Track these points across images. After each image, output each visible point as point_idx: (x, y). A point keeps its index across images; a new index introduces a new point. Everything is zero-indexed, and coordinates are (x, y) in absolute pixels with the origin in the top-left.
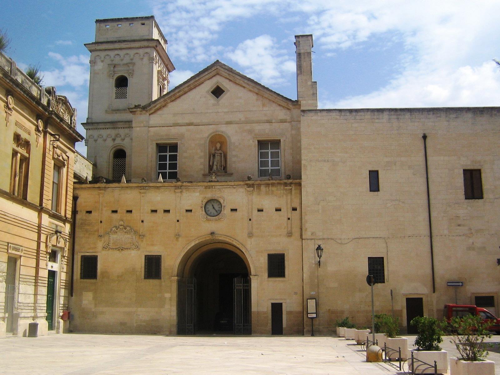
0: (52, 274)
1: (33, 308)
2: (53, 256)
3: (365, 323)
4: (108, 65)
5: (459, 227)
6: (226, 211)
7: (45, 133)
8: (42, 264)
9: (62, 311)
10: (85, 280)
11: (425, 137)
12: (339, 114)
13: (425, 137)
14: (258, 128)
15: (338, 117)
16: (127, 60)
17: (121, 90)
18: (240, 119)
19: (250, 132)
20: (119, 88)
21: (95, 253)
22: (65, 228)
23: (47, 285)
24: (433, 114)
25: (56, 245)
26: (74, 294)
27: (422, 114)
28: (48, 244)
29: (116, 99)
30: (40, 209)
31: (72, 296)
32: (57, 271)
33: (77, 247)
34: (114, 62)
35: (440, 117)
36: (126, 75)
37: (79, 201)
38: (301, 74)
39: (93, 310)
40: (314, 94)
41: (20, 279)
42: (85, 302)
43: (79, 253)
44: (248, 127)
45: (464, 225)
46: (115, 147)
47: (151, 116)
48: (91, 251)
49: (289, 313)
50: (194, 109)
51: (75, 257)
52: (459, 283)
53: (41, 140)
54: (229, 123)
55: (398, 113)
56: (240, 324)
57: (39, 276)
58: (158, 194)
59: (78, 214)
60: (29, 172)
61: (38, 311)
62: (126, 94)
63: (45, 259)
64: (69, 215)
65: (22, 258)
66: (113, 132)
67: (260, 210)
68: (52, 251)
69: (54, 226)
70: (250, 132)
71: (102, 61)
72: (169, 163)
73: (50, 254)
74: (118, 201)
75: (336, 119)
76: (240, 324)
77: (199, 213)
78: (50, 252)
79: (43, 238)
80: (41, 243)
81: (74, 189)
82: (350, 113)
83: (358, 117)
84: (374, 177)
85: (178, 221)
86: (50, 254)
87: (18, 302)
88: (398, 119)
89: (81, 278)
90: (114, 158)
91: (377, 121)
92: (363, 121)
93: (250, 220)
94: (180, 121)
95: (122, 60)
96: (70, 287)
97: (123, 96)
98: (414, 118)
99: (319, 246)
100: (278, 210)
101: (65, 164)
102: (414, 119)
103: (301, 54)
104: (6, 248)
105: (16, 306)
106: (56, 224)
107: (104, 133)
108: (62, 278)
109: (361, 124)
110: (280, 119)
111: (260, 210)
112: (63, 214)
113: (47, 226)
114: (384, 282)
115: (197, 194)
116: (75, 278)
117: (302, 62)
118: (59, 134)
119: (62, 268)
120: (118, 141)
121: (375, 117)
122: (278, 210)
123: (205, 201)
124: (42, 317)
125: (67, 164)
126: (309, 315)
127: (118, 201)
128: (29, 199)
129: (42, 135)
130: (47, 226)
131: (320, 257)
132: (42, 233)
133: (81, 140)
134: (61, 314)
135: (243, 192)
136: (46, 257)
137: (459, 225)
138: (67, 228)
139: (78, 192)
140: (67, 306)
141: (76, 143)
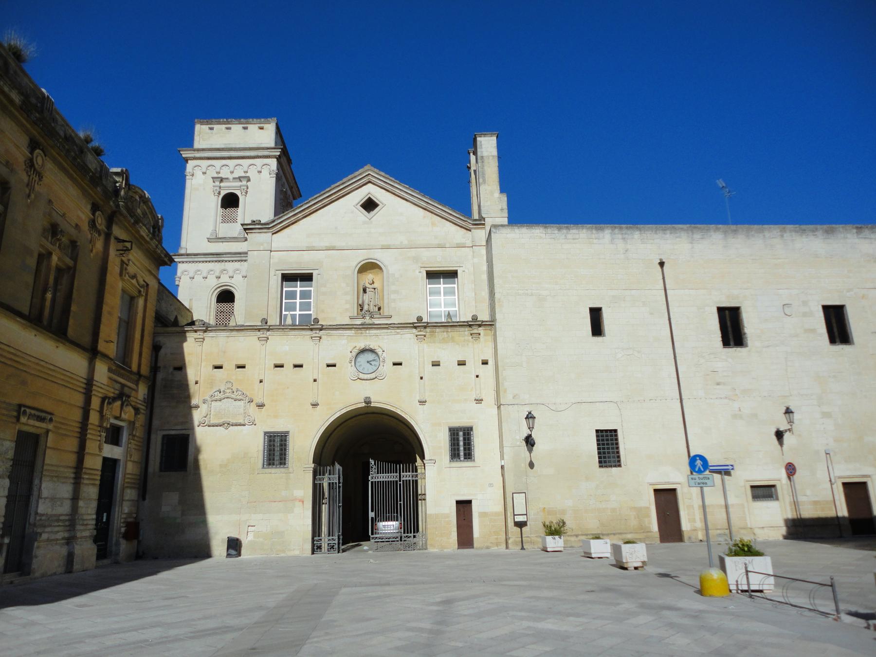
0: (110, 465)
1: (67, 523)
2: (114, 436)
3: (598, 528)
4: (213, 178)
5: (718, 387)
6: (387, 368)
7: (108, 236)
8: (91, 446)
9: (124, 525)
10: (166, 473)
11: (662, 264)
12: (544, 232)
13: (662, 264)
14: (426, 254)
15: (544, 236)
16: (239, 173)
17: (225, 306)
18: (402, 242)
19: (416, 259)
20: (227, 210)
21: (184, 431)
22: (137, 391)
23: (98, 482)
24: (671, 233)
25: (118, 415)
26: (147, 497)
27: (656, 233)
28: (104, 414)
29: (222, 224)
30: (93, 352)
31: (144, 499)
32: (119, 460)
33: (156, 423)
34: (220, 175)
35: (680, 237)
36: (238, 193)
37: (162, 352)
38: (485, 183)
39: (178, 521)
40: (503, 209)
41: (515, 517)
42: (165, 509)
43: (159, 432)
44: (413, 252)
45: (724, 384)
46: (219, 287)
47: (274, 235)
48: (179, 427)
49: (483, 515)
50: (336, 228)
51: (153, 437)
52: (727, 466)
53: (99, 245)
54: (388, 247)
55: (624, 232)
56: (409, 535)
57: (84, 467)
58: (285, 341)
59: (160, 371)
60: (74, 291)
61: (78, 527)
62: (229, 321)
63: (99, 438)
64: (145, 370)
65: (50, 434)
66: (217, 267)
67: (436, 364)
68: (110, 426)
69: (118, 386)
70: (416, 259)
71: (204, 173)
72: (300, 302)
73: (107, 430)
74: (225, 352)
75: (541, 238)
76: (409, 535)
77: (347, 369)
78: (108, 426)
79: (95, 403)
80: (92, 412)
81: (155, 334)
82: (558, 231)
83: (569, 236)
84: (596, 314)
85: (315, 381)
86: (107, 430)
87: (36, 513)
88: (625, 239)
89: (161, 470)
90: (217, 302)
91: (595, 241)
92: (577, 240)
93: (421, 378)
94: (317, 243)
95: (232, 172)
96: (143, 485)
97: (228, 310)
98: (645, 238)
99: (530, 413)
100: (462, 363)
101: (142, 293)
102: (645, 240)
103: (484, 158)
104: (15, 414)
105: (32, 520)
106: (120, 383)
107: (204, 267)
108: (128, 470)
109: (574, 245)
110: (457, 243)
111: (436, 364)
112: (134, 368)
113: (104, 385)
114: (620, 466)
115: (344, 342)
116: (150, 470)
117: (485, 168)
118: (131, 240)
119: (128, 453)
120: (225, 279)
121: (593, 236)
122: (462, 363)
123: (356, 351)
124: (86, 537)
125: (144, 294)
126: (515, 517)
127: (225, 352)
128: (71, 332)
129: (102, 238)
130: (104, 385)
131: (531, 428)
132: (94, 395)
133: (169, 263)
134: (123, 530)
135: (410, 339)
136: (100, 436)
137: (718, 384)
138: (142, 391)
139: (161, 339)
140: (135, 515)
141: (161, 268)
